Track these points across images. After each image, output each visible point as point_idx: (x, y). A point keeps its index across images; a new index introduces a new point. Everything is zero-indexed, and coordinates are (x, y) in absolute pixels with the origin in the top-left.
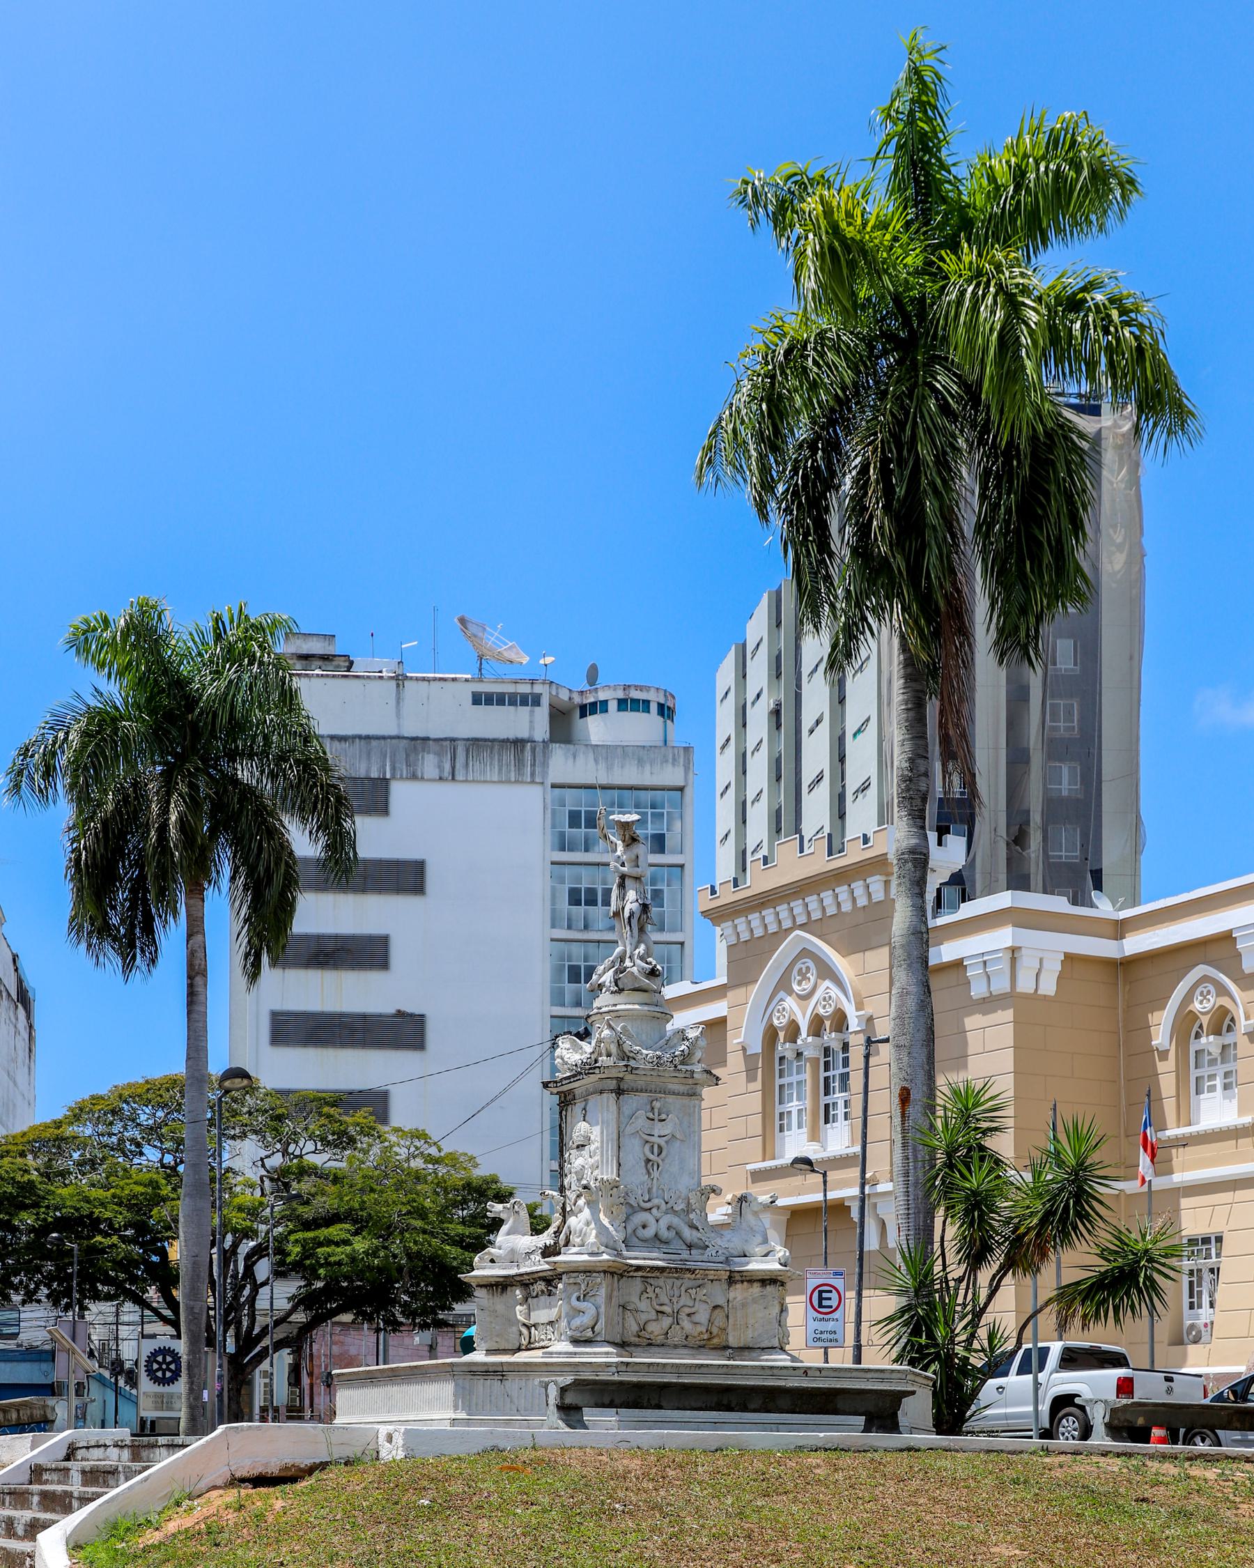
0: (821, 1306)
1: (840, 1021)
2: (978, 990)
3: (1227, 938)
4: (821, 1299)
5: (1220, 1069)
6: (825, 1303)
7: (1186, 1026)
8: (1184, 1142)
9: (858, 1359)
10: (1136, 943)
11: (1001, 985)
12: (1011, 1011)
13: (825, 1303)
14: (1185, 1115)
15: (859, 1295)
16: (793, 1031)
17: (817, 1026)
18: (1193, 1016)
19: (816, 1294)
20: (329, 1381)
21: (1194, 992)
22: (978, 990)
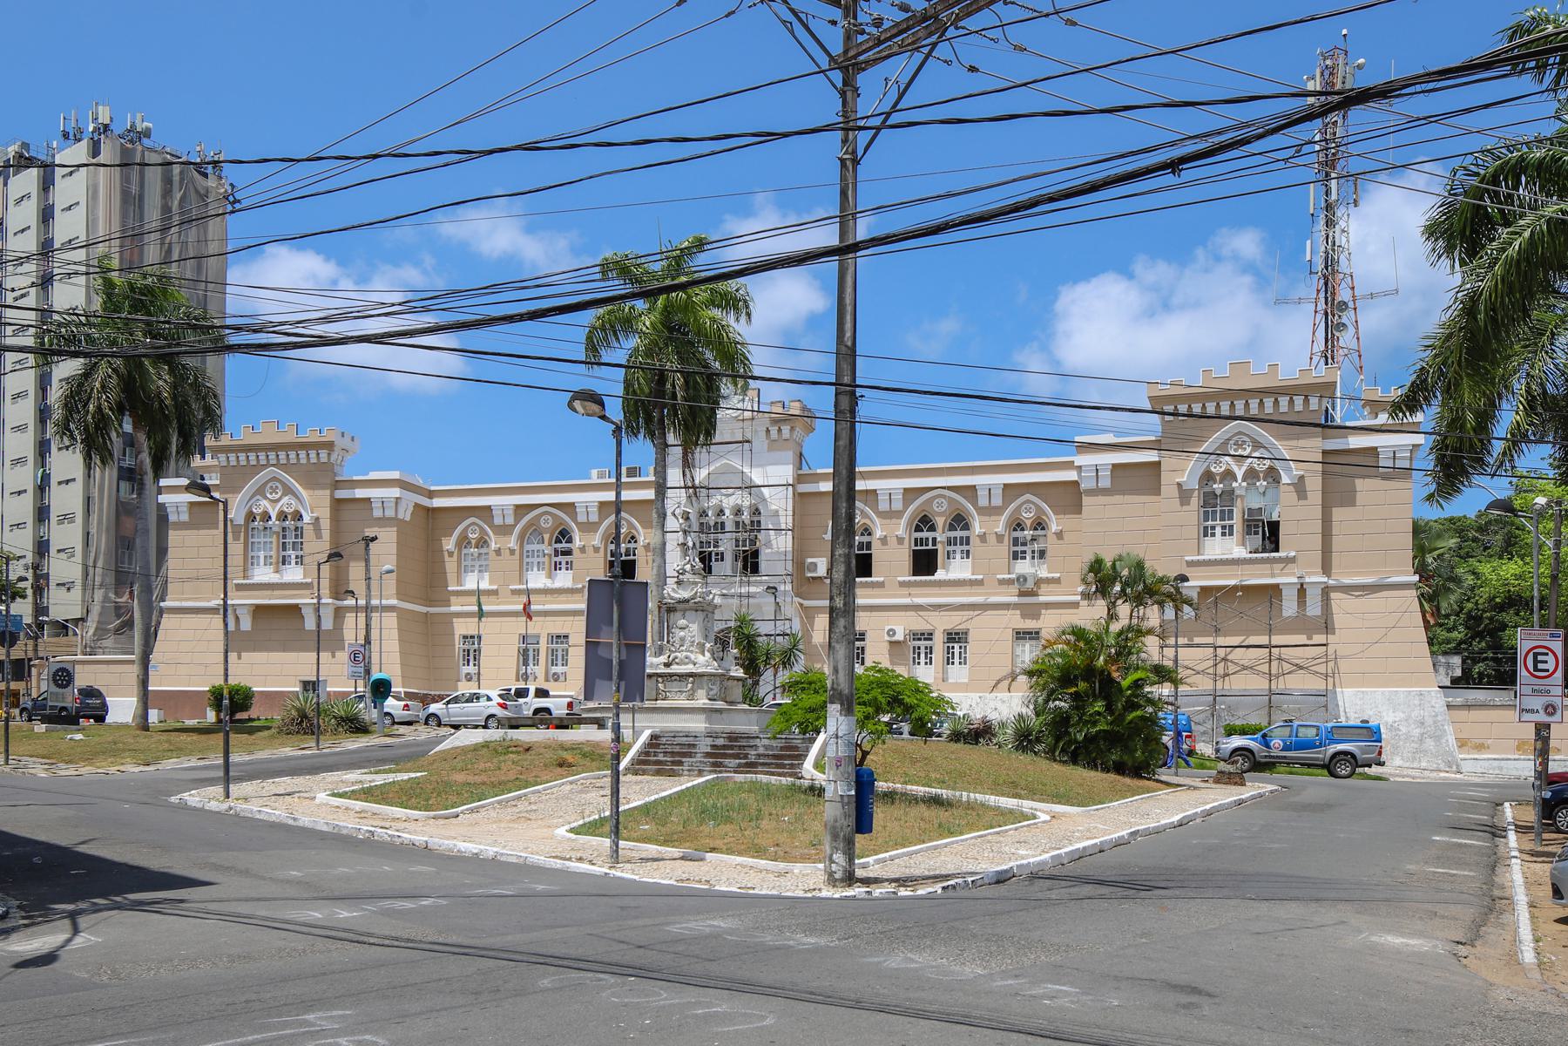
0: (1536, 669)
1: (298, 516)
2: (377, 513)
3: (489, 508)
4: (1536, 662)
5: (477, 564)
6: (1540, 666)
7: (463, 542)
8: (458, 593)
9: (650, 676)
10: (438, 502)
11: (390, 513)
12: (408, 518)
13: (1540, 666)
14: (459, 583)
15: (319, 625)
16: (266, 517)
17: (283, 516)
18: (466, 537)
19: (1531, 656)
20: (161, 611)
21: (471, 527)
22: (377, 513)
